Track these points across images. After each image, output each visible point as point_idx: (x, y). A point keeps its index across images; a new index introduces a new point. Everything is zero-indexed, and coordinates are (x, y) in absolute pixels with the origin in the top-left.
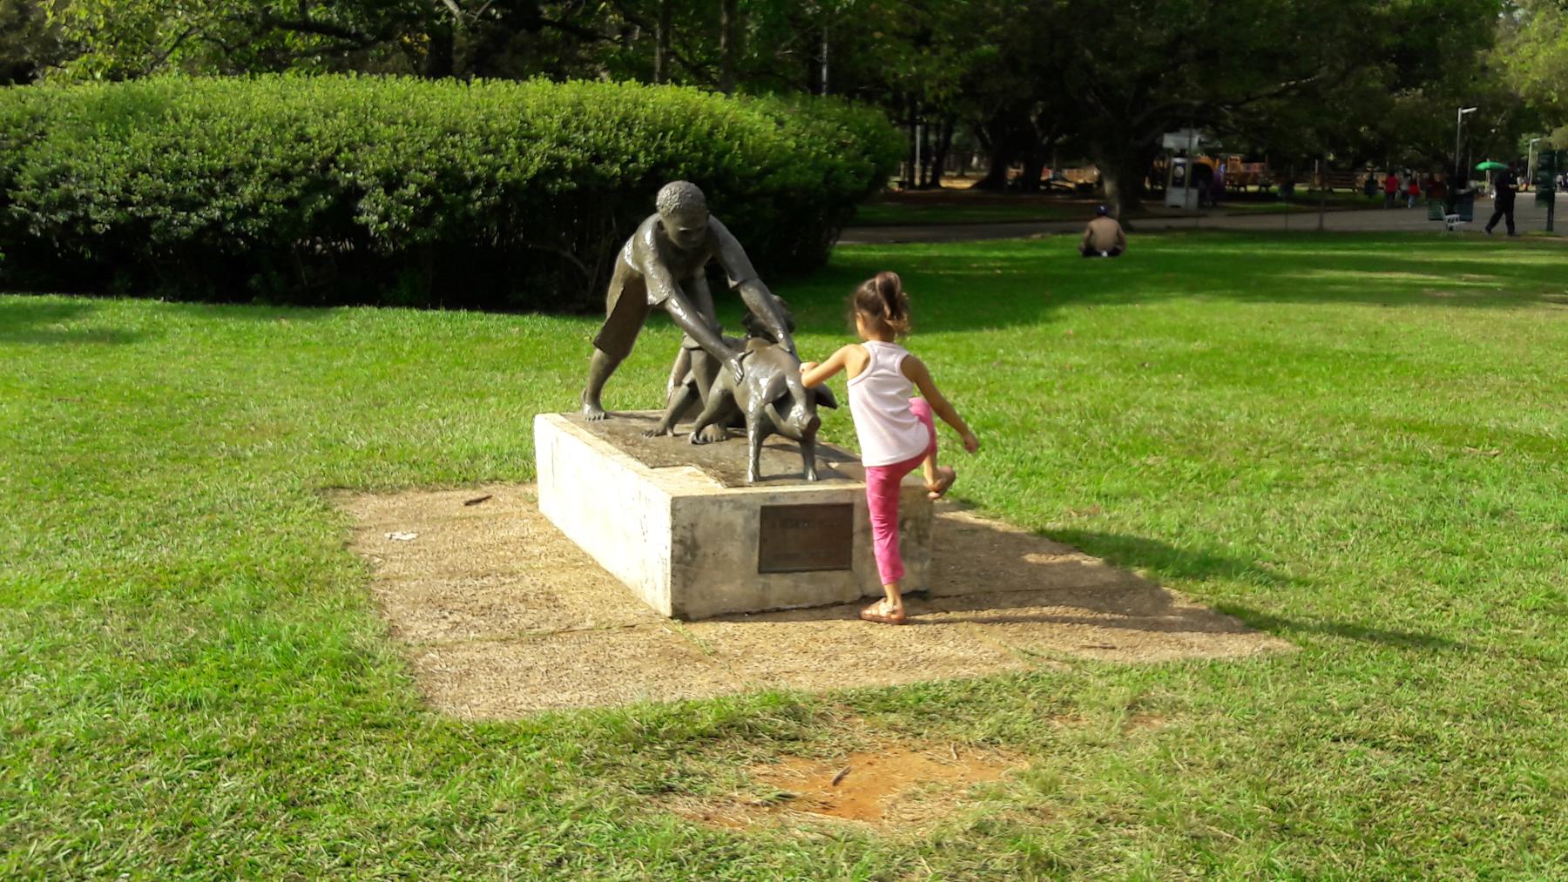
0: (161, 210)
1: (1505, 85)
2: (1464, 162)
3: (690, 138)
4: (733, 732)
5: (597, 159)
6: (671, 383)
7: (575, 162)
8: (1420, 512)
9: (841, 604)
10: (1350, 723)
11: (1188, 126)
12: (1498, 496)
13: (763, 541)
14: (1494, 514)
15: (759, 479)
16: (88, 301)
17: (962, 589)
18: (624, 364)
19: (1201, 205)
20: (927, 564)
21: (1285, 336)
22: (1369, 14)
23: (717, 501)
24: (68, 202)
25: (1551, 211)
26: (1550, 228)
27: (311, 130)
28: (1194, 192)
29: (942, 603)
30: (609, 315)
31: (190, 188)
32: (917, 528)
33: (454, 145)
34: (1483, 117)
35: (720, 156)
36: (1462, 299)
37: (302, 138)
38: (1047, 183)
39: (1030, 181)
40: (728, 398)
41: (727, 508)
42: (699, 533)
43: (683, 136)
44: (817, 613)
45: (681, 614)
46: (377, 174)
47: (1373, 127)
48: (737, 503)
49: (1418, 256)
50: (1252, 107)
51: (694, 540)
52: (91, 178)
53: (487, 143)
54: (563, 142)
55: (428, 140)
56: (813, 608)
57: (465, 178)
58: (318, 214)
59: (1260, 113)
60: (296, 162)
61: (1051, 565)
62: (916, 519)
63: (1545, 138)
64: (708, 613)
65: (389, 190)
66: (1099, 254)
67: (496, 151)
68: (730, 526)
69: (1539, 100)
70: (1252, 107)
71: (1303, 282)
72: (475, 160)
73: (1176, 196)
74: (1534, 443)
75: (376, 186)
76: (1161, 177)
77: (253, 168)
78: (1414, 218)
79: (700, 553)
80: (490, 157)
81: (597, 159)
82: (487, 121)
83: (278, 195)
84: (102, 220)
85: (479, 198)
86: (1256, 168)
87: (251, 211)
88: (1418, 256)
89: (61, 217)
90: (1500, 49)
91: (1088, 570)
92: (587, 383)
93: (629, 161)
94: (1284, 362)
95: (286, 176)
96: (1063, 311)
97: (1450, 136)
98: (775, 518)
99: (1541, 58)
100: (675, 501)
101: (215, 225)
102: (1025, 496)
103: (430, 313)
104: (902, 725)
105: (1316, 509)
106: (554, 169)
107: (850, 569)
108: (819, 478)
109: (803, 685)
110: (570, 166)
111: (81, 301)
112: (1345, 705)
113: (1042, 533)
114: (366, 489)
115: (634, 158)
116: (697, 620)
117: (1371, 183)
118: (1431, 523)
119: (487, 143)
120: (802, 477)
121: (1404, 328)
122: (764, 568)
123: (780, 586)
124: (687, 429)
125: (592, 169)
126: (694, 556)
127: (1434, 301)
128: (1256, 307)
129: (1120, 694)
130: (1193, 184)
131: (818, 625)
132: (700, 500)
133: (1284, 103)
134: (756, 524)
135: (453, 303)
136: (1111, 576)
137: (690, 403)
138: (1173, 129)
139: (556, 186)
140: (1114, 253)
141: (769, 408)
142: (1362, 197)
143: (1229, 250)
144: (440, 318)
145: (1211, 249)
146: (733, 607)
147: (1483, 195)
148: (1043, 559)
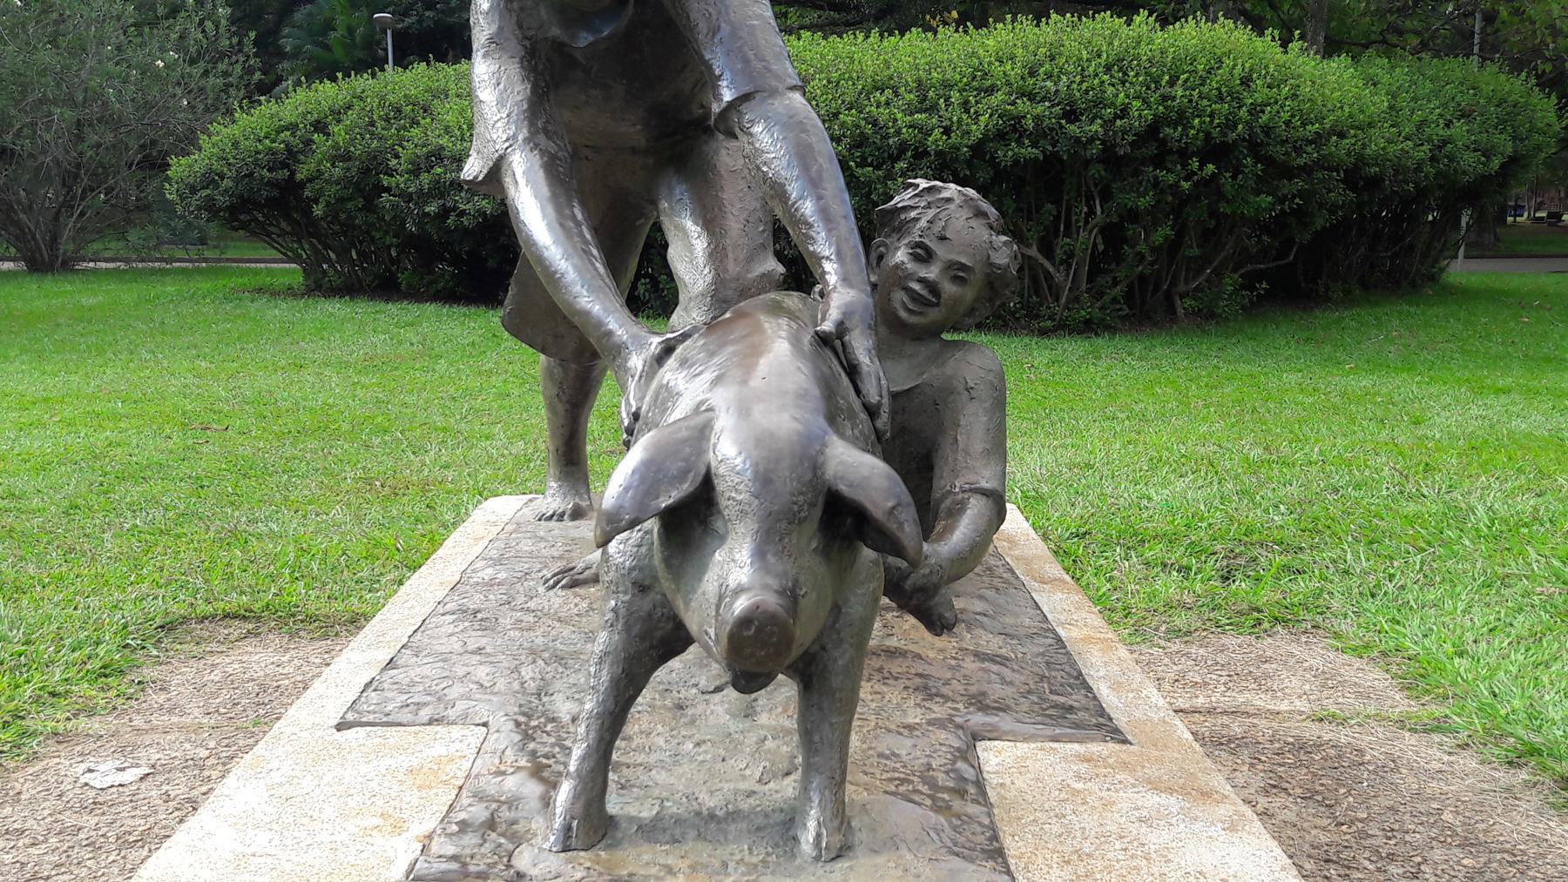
7: (1038, 119)
35: (1255, 111)
81: (1072, 115)
106: (1011, 129)
115: (1124, 112)
139: (1007, 154)
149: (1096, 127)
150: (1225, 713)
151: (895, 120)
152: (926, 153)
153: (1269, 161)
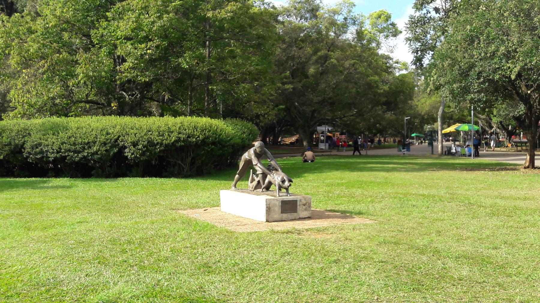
0: (70, 154)
1: (418, 111)
2: (407, 134)
5: (189, 137)
8: (399, 206)
11: (324, 124)
12: (414, 203)
16: (48, 179)
19: (329, 148)
23: (274, 200)
24: (42, 152)
26: (432, 153)
27: (110, 131)
28: (327, 144)
30: (240, 168)
31: (78, 147)
34: (412, 120)
35: (220, 135)
36: (407, 170)
37: (108, 134)
38: (280, 142)
40: (270, 183)
43: (210, 131)
45: (267, 221)
47: (380, 124)
48: (277, 200)
49: (395, 161)
50: (345, 119)
52: (48, 145)
53: (159, 134)
54: (179, 133)
55: (144, 133)
58: (114, 154)
59: (347, 121)
60: (107, 140)
63: (432, 126)
65: (134, 146)
67: (163, 135)
68: (276, 204)
69: (428, 115)
70: (345, 119)
71: (366, 168)
72: (157, 138)
73: (322, 146)
76: (318, 140)
77: (96, 142)
78: (394, 151)
83: (104, 148)
84: (52, 157)
86: (343, 137)
87: (96, 153)
88: (395, 161)
89: (39, 156)
90: (416, 100)
94: (366, 184)
95: (105, 144)
96: (306, 175)
97: (402, 126)
99: (427, 103)
101: (84, 157)
102: (321, 205)
103: (145, 179)
105: (378, 206)
106: (178, 140)
111: (45, 179)
115: (199, 137)
117: (380, 141)
118: (401, 207)
119: (159, 134)
121: (393, 177)
122: (282, 213)
123: (285, 216)
127: (400, 171)
128: (355, 173)
130: (327, 142)
133: (354, 117)
138: (320, 125)
141: (281, 183)
144: (147, 179)
145: (337, 160)
147: (414, 144)
149: (194, 140)
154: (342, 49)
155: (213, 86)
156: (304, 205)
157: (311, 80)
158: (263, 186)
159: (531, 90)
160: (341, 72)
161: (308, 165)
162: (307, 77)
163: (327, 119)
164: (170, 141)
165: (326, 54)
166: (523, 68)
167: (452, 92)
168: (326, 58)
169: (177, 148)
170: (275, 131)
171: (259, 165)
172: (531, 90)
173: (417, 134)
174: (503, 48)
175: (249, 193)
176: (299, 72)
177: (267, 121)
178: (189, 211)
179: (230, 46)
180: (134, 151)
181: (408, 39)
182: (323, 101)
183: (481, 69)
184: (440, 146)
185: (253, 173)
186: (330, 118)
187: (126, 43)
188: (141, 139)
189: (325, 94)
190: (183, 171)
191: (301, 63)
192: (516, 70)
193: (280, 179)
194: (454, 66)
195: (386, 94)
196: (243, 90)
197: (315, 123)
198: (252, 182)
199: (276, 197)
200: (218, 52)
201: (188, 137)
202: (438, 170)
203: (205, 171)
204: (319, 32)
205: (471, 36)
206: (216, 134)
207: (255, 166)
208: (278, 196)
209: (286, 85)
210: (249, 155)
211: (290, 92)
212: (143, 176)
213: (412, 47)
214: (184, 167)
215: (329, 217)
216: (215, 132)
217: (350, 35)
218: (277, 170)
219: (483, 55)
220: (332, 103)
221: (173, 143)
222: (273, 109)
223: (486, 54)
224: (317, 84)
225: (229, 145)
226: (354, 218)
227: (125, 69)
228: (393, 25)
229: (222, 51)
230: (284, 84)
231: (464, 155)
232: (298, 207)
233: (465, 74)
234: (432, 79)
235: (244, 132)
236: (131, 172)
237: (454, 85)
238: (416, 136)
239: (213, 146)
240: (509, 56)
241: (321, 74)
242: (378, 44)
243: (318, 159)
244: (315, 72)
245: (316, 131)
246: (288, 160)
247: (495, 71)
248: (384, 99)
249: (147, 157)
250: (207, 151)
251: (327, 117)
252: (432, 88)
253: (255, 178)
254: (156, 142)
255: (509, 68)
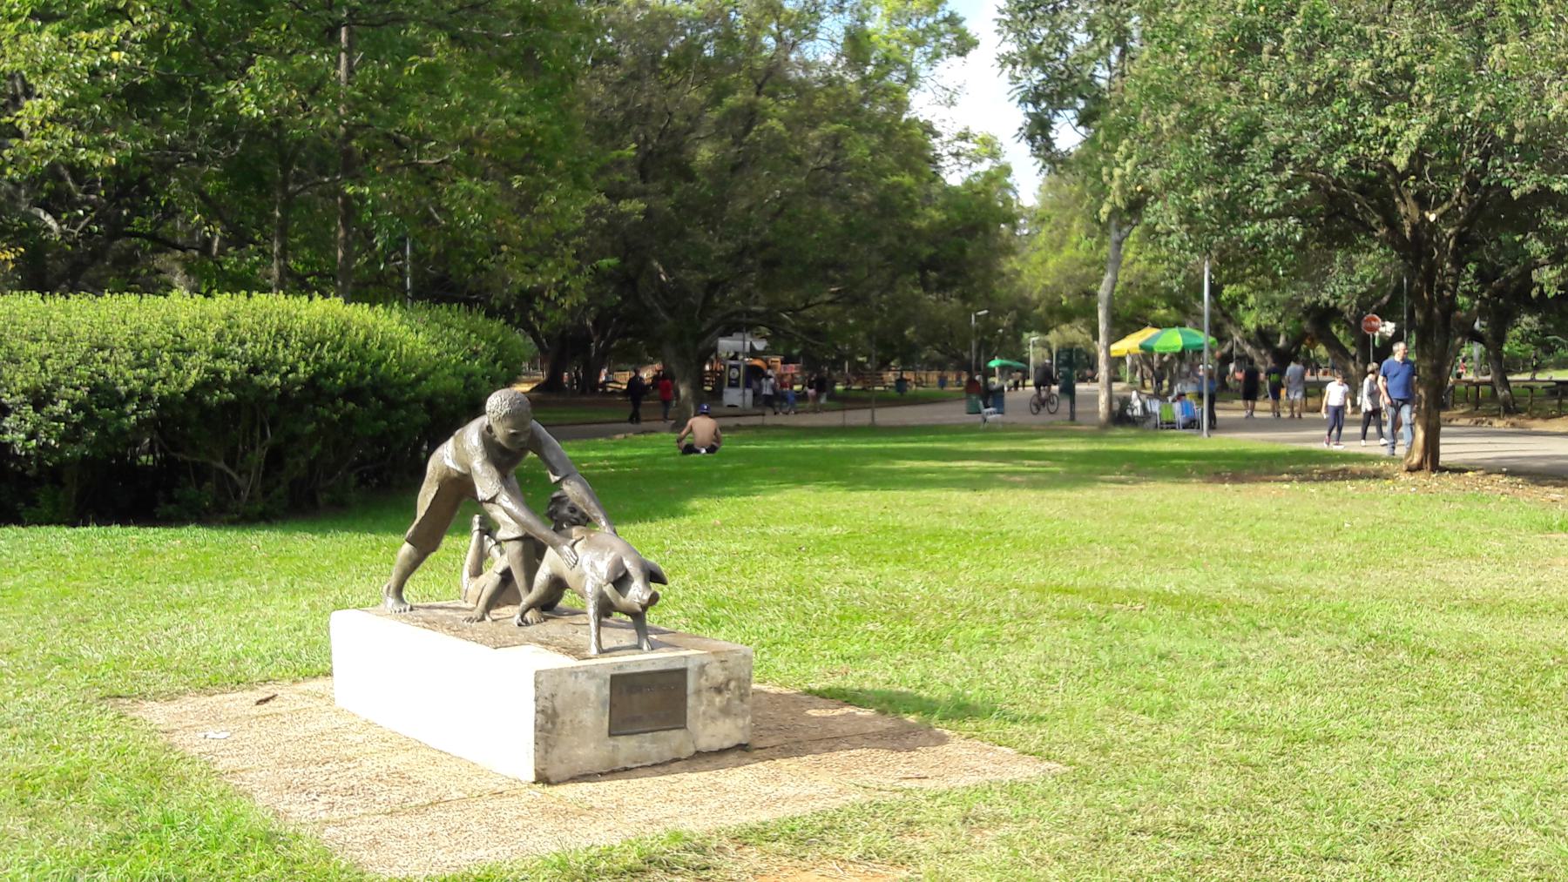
3: (346, 348)
4: (653, 867)
5: (255, 370)
6: (466, 574)
7: (234, 374)
9: (678, 760)
10: (1136, 821)
11: (739, 330)
12: (1163, 645)
13: (612, 706)
14: (1161, 657)
15: (602, 651)
17: (773, 741)
18: (432, 557)
20: (749, 718)
21: (903, 518)
22: (911, 227)
23: (573, 672)
25: (1073, 402)
28: (749, 392)
29: (763, 753)
32: (739, 688)
33: (105, 361)
35: (378, 363)
36: (1035, 485)
38: (604, 385)
39: (589, 385)
40: (558, 585)
41: (582, 678)
42: (558, 703)
43: (340, 347)
44: (659, 769)
45: (543, 779)
46: (25, 391)
48: (591, 674)
49: (972, 446)
51: (554, 710)
53: (138, 357)
54: (219, 355)
55: (77, 356)
56: (655, 765)
57: (118, 393)
61: (834, 718)
62: (738, 679)
64: (567, 776)
65: (37, 407)
66: (698, 452)
67: (151, 364)
68: (584, 696)
70: (809, 312)
72: (129, 374)
73: (732, 396)
74: (1162, 599)
75: (24, 403)
79: (559, 720)
80: (144, 371)
81: (255, 370)
82: (137, 335)
85: (134, 412)
88: (972, 446)
91: (868, 719)
92: (393, 580)
93: (288, 372)
96: (696, 503)
98: (624, 686)
99: (1051, 264)
100: (537, 674)
103: (82, 530)
104: (788, 850)
105: (1025, 660)
106: (213, 381)
107: (685, 727)
108: (654, 646)
109: (696, 825)
110: (228, 378)
112: (1127, 807)
113: (810, 692)
114: (144, 696)
115: (294, 369)
116: (558, 783)
119: (138, 357)
120: (639, 647)
122: (612, 733)
123: (628, 747)
124: (511, 612)
125: (250, 381)
126: (554, 724)
127: (1014, 485)
128: (866, 494)
129: (952, 812)
130: (748, 385)
131: (669, 778)
132: (560, 672)
134: (606, 691)
135: (104, 519)
136: (885, 723)
137: (505, 589)
138: (727, 333)
140: (711, 450)
141: (609, 589)
142: (893, 393)
143: (804, 445)
144: (92, 533)
146: (587, 769)
148: (824, 713)
149: (276, 380)
150: (1473, 606)
151: (122, 375)
152: (150, 397)
153: (384, 398)
154: (802, 89)
155: (362, 185)
156: (719, 690)
157: (704, 186)
158: (527, 599)
159: (1440, 210)
160: (798, 160)
161: (699, 463)
162: (686, 174)
163: (757, 314)
164: (181, 385)
165: (751, 105)
166: (1433, 136)
167: (1189, 216)
168: (750, 116)
169: (206, 412)
170: (588, 350)
171: (504, 499)
172: (1440, 210)
173: (1005, 362)
174: (1366, 65)
175: (458, 632)
176: (663, 161)
177: (557, 316)
178: (192, 704)
179: (428, 52)
180: (37, 426)
181: (1007, 60)
182: (743, 252)
183: (1287, 136)
184: (1103, 398)
185: (482, 532)
186: (761, 309)
187: (39, 30)
188: (63, 377)
189: (747, 233)
190: (237, 496)
191: (673, 134)
192: (1413, 136)
193: (604, 567)
194: (1193, 129)
195: (937, 235)
196: (469, 201)
197: (713, 328)
198: (477, 572)
199: (590, 655)
200: (383, 71)
201: (250, 370)
202: (1135, 482)
203: (323, 498)
204: (728, 38)
205: (1251, 26)
206: (361, 357)
207: (488, 506)
208: (593, 651)
209: (622, 203)
210: (460, 452)
211: (637, 223)
212: (75, 518)
213: (1023, 82)
214: (241, 482)
215: (829, 740)
216: (360, 352)
217: (822, 50)
218: (585, 521)
219: (1292, 87)
220: (770, 262)
221: (190, 394)
222: (579, 270)
223: (1304, 86)
224: (722, 201)
225: (416, 400)
226: (942, 740)
227: (32, 124)
228: (953, 20)
229: (399, 67)
230: (615, 195)
231: (1171, 425)
232: (691, 701)
233: (1230, 155)
234: (1117, 172)
235: (476, 353)
236: (32, 502)
237: (1198, 193)
238: (1002, 368)
239: (351, 405)
240: (1389, 89)
241: (735, 168)
242: (911, 78)
243: (729, 444)
244: (716, 160)
245: (715, 350)
246: (631, 446)
247: (1334, 143)
248: (927, 251)
249: (90, 445)
250: (331, 423)
251: (754, 308)
252: (1119, 203)
253: (495, 551)
254: (123, 389)
255: (1386, 130)
